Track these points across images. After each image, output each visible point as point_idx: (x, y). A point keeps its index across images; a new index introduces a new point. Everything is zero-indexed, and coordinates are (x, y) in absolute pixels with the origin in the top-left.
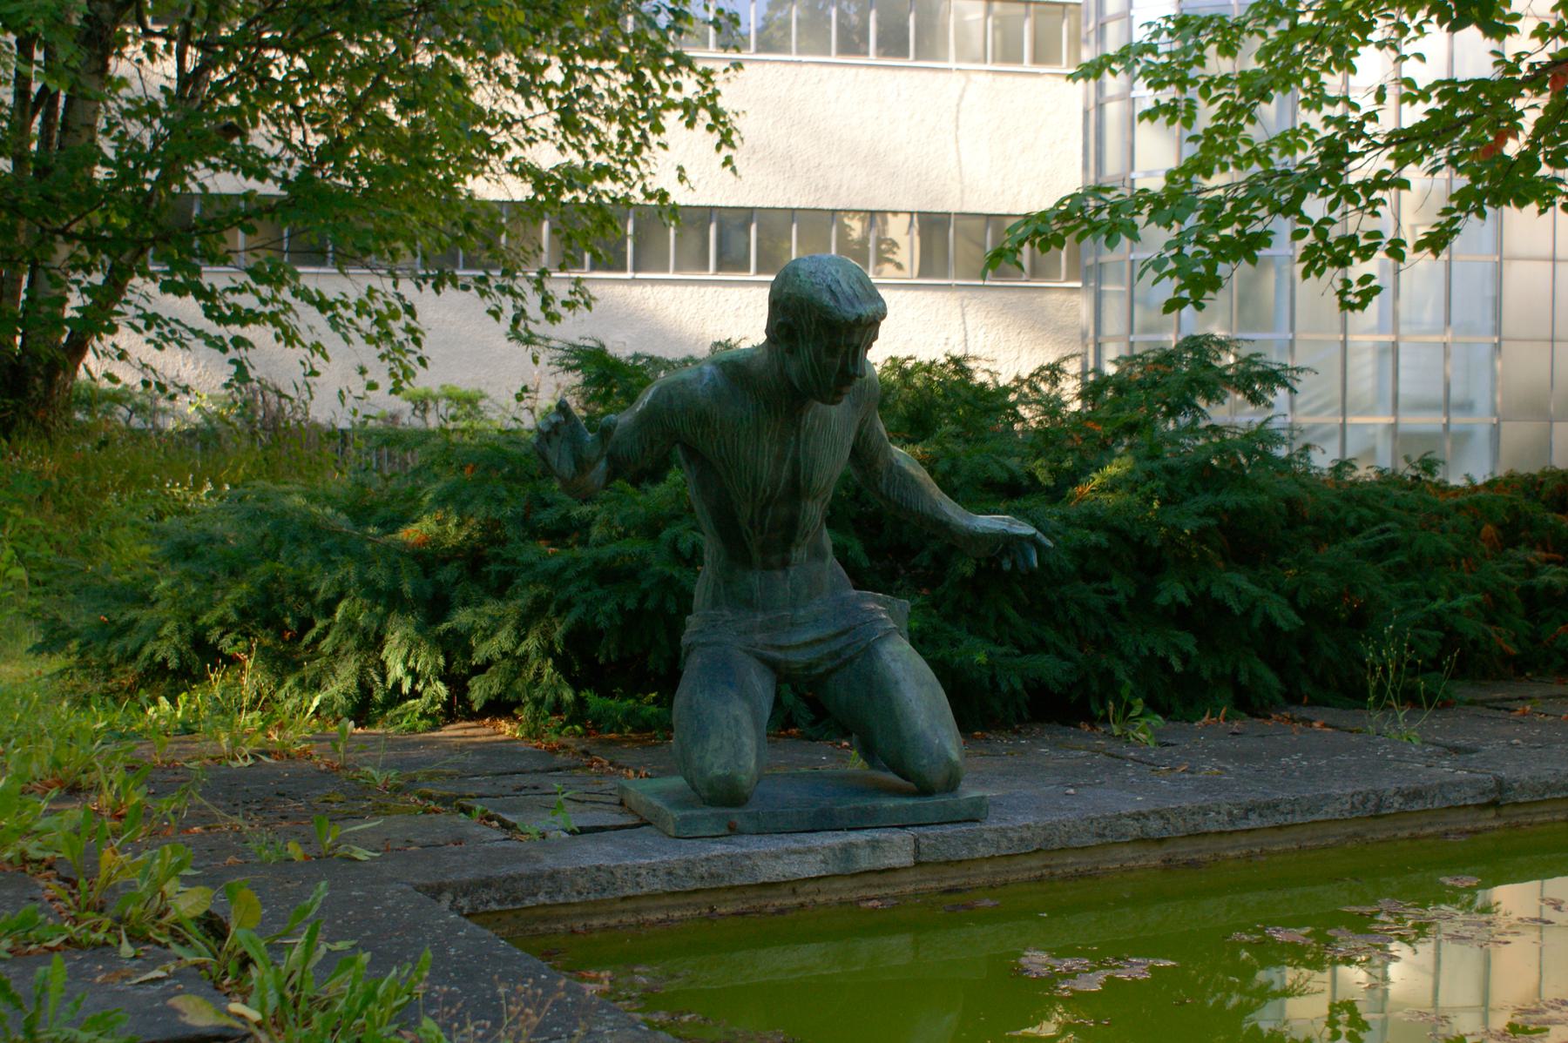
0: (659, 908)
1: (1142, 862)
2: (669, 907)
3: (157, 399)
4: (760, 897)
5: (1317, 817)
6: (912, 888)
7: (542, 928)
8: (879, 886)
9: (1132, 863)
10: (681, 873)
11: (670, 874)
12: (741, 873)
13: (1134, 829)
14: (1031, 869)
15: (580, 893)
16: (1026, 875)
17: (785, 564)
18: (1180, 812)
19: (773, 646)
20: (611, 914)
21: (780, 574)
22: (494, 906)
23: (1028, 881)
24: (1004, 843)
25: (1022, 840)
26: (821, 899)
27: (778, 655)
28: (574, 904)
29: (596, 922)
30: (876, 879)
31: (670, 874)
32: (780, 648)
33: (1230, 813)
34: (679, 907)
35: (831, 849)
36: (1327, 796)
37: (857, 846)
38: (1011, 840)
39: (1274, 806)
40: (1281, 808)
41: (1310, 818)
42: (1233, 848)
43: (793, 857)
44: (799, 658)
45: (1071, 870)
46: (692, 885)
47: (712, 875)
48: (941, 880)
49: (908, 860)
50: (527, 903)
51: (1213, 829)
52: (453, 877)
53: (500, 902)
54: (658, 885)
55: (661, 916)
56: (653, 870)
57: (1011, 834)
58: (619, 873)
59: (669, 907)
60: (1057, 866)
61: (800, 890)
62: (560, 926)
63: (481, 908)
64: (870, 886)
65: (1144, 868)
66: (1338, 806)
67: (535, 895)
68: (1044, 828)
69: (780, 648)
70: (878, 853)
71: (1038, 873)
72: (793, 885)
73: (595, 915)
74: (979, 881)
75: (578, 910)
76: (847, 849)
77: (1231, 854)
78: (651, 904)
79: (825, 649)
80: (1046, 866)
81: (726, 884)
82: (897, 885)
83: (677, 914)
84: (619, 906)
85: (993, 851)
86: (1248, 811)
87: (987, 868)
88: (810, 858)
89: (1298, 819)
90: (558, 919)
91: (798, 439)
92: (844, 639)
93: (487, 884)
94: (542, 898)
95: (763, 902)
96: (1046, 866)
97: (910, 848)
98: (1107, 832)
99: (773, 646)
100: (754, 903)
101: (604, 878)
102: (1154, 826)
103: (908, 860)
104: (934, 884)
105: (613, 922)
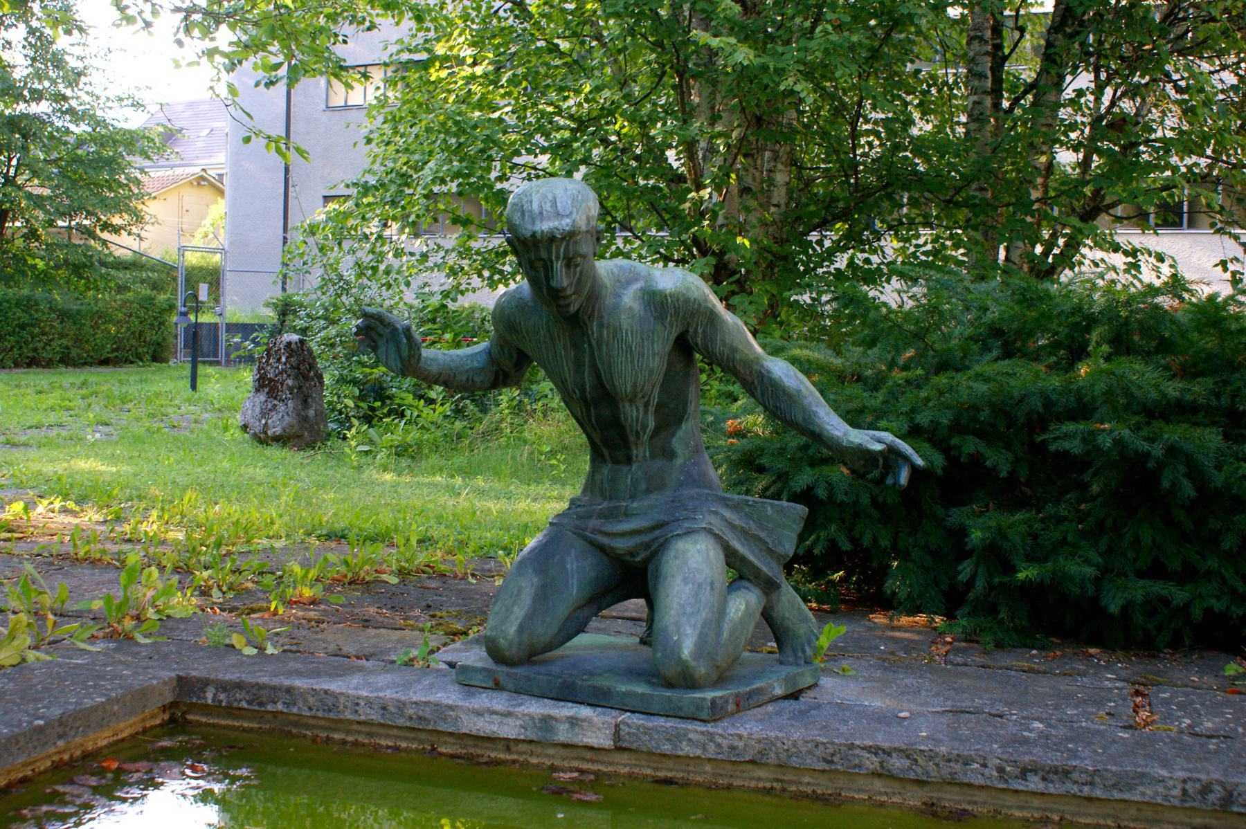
0: (387, 736)
1: (896, 799)
2: (398, 737)
3: (670, 147)
4: (476, 746)
5: (1126, 796)
6: (627, 770)
7: (294, 731)
8: (593, 761)
9: (884, 798)
10: (393, 710)
11: (384, 708)
12: (445, 720)
13: (872, 762)
14: (759, 779)
15: (310, 709)
16: (753, 784)
17: (629, 461)
18: (931, 755)
19: (601, 532)
20: (348, 732)
21: (625, 469)
22: (244, 704)
23: (757, 790)
24: (711, 747)
25: (732, 748)
26: (534, 760)
27: (605, 541)
28: (319, 718)
29: (336, 736)
30: (589, 755)
31: (384, 708)
32: (607, 534)
33: (1001, 770)
34: (405, 739)
35: (532, 718)
36: (1143, 775)
37: (556, 720)
38: (719, 745)
39: (1066, 773)
40: (1075, 776)
41: (1116, 795)
42: (1021, 808)
43: (495, 717)
44: (621, 545)
45: (809, 790)
46: (401, 722)
47: (420, 718)
48: (657, 769)
49: (608, 743)
50: (270, 708)
51: (976, 783)
52: (221, 676)
53: (249, 703)
54: (375, 716)
55: (390, 744)
56: (369, 702)
57: (719, 740)
58: (342, 700)
59: (398, 737)
60: (790, 782)
61: (514, 749)
62: (309, 733)
63: (235, 704)
64: (583, 759)
65: (899, 806)
66: (1160, 789)
67: (275, 703)
68: (759, 741)
69: (607, 534)
70: (577, 730)
71: (768, 785)
72: (508, 744)
73: (335, 730)
74: (699, 779)
75: (322, 723)
76: (546, 721)
77: (1017, 813)
78: (382, 731)
79: (639, 539)
80: (777, 780)
81: (430, 727)
82: (611, 764)
83: (404, 745)
84: (355, 727)
85: (698, 752)
86: (1024, 772)
87: (708, 768)
88: (510, 721)
89: (1099, 793)
90: (308, 727)
91: (590, 345)
92: (657, 533)
93: (240, 685)
94: (280, 707)
95: (479, 752)
96: (777, 780)
97: (609, 732)
98: (836, 759)
99: (601, 532)
100: (472, 750)
101: (330, 701)
102: (897, 763)
103: (608, 743)
104: (649, 772)
105: (350, 739)
